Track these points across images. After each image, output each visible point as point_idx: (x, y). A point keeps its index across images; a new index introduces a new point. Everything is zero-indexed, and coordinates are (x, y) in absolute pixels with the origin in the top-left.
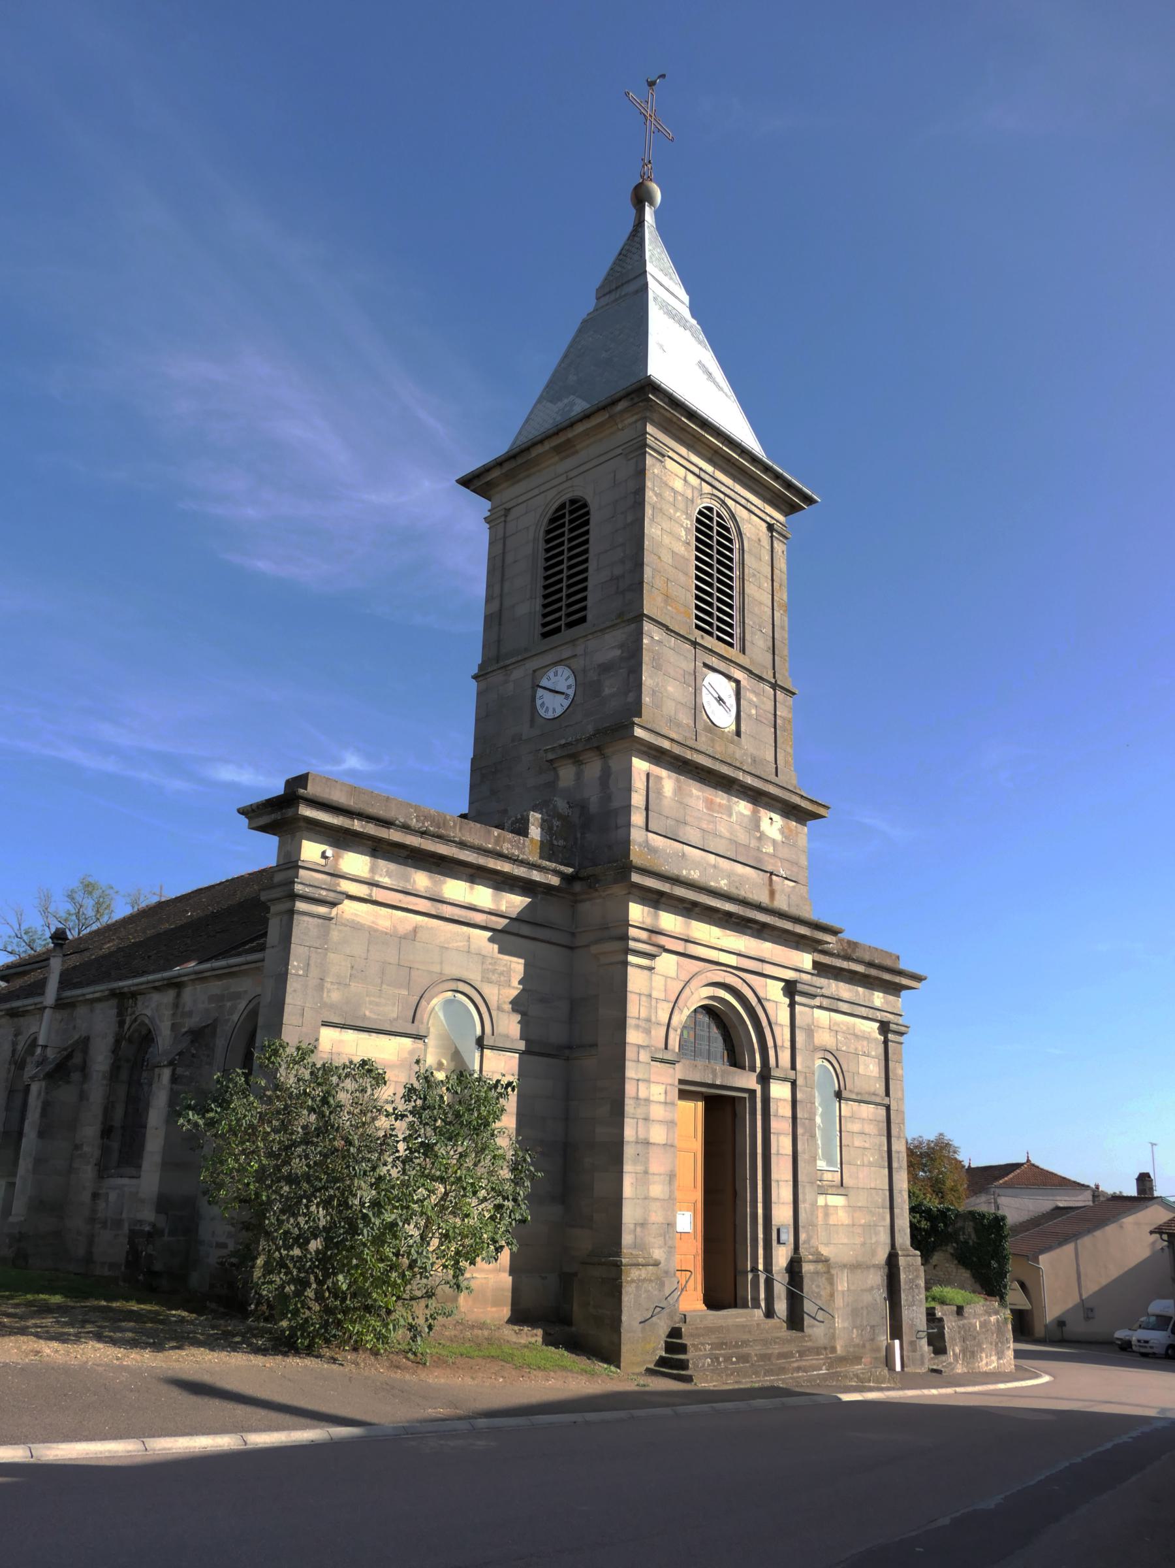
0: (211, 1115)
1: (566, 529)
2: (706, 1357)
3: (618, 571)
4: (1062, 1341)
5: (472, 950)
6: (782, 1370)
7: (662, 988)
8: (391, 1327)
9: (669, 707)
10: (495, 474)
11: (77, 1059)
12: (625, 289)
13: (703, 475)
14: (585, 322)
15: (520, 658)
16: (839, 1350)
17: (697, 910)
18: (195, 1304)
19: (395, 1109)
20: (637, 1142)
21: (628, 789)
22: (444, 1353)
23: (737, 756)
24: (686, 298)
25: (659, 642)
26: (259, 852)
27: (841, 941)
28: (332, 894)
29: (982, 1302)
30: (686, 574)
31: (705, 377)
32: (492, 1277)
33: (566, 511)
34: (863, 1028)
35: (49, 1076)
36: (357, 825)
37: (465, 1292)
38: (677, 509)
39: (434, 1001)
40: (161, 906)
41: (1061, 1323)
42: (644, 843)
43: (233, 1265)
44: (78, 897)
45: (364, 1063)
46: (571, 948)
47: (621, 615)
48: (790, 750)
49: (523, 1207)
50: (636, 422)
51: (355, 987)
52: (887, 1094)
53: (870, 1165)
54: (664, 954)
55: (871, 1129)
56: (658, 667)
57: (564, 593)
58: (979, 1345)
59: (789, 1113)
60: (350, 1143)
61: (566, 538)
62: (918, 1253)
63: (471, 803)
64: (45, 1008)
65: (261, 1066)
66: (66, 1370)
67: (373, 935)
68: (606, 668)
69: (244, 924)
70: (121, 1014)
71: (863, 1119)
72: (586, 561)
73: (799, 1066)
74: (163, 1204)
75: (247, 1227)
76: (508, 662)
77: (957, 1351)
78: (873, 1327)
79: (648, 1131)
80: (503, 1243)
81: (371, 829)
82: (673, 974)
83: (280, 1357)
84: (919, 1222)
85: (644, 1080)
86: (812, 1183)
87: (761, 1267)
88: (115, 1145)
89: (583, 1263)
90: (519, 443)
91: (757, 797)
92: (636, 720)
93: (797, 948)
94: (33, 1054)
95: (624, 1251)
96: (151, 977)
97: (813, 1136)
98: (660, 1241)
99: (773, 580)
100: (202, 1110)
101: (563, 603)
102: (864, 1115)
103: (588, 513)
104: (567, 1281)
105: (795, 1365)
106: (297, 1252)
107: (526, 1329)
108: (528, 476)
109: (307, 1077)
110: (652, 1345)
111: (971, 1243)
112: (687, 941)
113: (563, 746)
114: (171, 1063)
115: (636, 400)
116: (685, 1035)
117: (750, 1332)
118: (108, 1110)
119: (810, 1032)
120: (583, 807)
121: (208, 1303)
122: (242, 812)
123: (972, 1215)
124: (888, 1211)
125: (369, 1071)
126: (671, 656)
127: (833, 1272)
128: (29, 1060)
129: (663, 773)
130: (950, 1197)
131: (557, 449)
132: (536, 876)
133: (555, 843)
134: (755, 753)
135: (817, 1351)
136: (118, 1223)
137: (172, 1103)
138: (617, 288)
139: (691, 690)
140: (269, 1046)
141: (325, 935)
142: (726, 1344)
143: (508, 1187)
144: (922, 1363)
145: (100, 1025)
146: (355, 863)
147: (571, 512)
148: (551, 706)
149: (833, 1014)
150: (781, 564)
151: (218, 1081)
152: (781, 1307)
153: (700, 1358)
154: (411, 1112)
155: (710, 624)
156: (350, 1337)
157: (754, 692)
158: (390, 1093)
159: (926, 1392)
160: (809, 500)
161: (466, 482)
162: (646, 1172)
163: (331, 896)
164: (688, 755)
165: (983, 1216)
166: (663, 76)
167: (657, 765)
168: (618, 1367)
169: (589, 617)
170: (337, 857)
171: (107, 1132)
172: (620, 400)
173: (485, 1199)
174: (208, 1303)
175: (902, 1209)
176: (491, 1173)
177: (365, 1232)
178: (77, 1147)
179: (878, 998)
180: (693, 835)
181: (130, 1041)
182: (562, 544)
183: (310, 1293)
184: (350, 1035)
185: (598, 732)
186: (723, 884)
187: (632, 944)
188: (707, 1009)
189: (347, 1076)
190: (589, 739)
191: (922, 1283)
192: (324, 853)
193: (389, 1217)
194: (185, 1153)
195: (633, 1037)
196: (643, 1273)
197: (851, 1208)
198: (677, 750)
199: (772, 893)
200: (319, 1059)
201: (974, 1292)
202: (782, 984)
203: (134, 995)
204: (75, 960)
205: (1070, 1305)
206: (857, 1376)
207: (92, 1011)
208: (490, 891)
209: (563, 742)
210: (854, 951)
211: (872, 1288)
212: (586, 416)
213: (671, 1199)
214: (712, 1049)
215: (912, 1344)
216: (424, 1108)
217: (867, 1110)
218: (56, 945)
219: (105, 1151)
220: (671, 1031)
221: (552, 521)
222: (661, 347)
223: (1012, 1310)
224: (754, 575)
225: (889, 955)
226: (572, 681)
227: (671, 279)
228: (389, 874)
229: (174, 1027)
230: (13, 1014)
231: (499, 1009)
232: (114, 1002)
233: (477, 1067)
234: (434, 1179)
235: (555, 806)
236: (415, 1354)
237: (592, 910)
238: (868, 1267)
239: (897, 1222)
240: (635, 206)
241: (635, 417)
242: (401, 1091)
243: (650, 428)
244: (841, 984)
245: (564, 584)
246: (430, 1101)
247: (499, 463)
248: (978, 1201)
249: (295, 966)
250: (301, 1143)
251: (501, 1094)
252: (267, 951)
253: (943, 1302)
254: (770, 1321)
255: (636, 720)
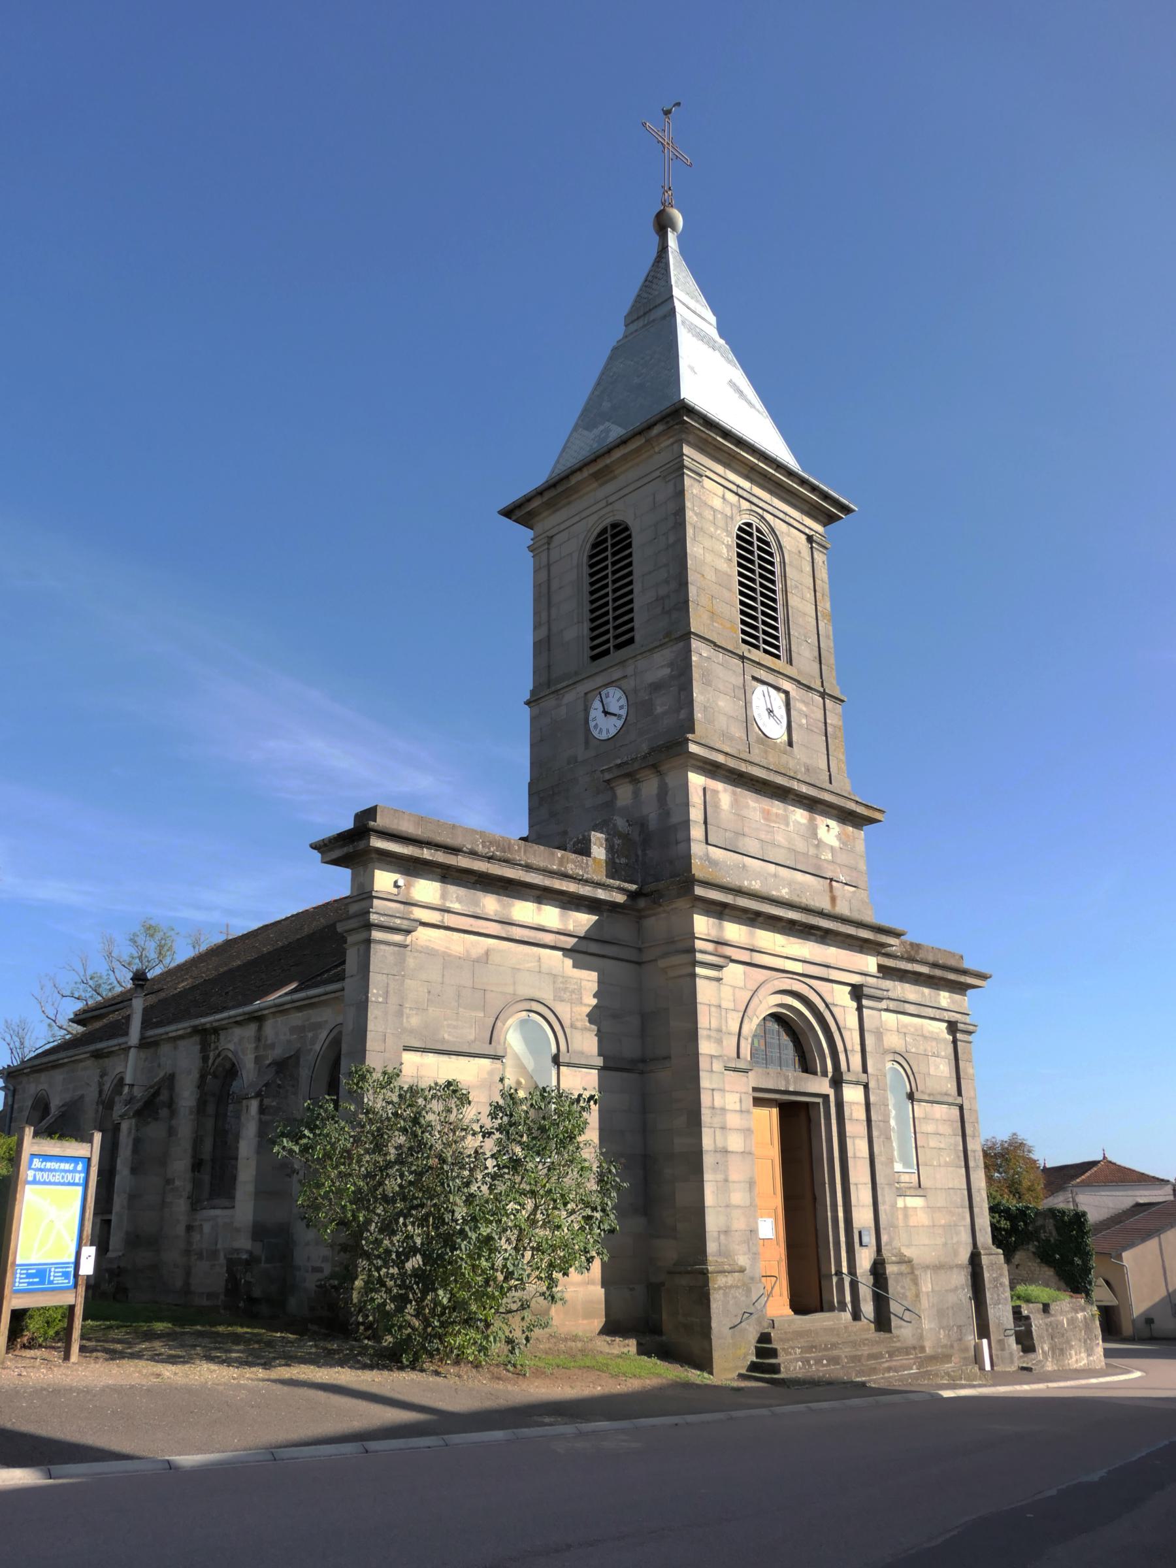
0: (305, 1141)
1: (609, 553)
2: (797, 1360)
3: (663, 591)
4: (1152, 1339)
5: (543, 970)
6: (874, 1370)
7: (731, 998)
8: (491, 1339)
9: (721, 722)
10: (535, 503)
11: (164, 1096)
12: (653, 314)
13: (741, 492)
14: (615, 349)
15: (571, 682)
16: (928, 1345)
17: (761, 919)
18: (300, 1326)
19: (481, 1127)
20: (716, 1151)
21: (686, 805)
22: (541, 1364)
23: (791, 765)
24: (713, 319)
25: (708, 658)
26: (336, 883)
27: (903, 943)
28: (406, 922)
29: (1068, 1299)
30: (730, 590)
31: (737, 395)
32: (584, 1288)
33: (608, 535)
34: (931, 1029)
35: (138, 1114)
36: (427, 854)
37: (560, 1303)
38: (717, 527)
39: (510, 1022)
40: (229, 944)
41: (1149, 1321)
42: (706, 856)
43: (334, 1287)
44: (141, 940)
45: (449, 1084)
46: (639, 963)
47: (668, 634)
48: (843, 757)
49: (612, 1216)
50: (672, 444)
51: (434, 1012)
52: (960, 1093)
53: (947, 1165)
54: (732, 965)
55: (946, 1129)
56: (708, 683)
57: (611, 616)
58: (1068, 1342)
59: (863, 1116)
60: (443, 1161)
61: (609, 562)
62: (1000, 1251)
63: (531, 826)
64: (130, 1048)
65: (350, 1092)
66: (188, 1390)
67: (447, 961)
68: (656, 687)
69: (322, 953)
70: (205, 1048)
71: (937, 1120)
72: (631, 583)
73: (870, 1070)
74: (259, 1232)
75: (344, 1248)
76: (559, 686)
77: (1046, 1348)
78: (959, 1327)
79: (726, 1139)
80: (594, 1254)
81: (440, 857)
82: (741, 984)
83: (386, 1373)
84: (999, 1222)
85: (719, 1090)
86: (890, 1185)
87: (845, 1270)
88: (206, 1178)
89: (669, 1273)
90: (557, 471)
91: (812, 804)
92: (690, 736)
93: (861, 952)
94: (121, 1094)
95: (710, 1258)
96: (232, 1013)
97: (889, 1138)
98: (744, 1248)
99: (815, 591)
100: (296, 1137)
101: (611, 626)
102: (938, 1116)
103: (629, 536)
104: (654, 1291)
105: (886, 1365)
106: (394, 1271)
107: (618, 1339)
108: (569, 503)
109: (395, 1099)
110: (743, 1351)
111: (1052, 1240)
112: (752, 950)
113: (619, 766)
114: (258, 1095)
115: (671, 423)
116: (756, 1044)
117: (838, 1335)
118: (197, 1142)
119: (879, 1035)
120: (642, 824)
121: (309, 1326)
122: (314, 847)
123: (1052, 1213)
124: (967, 1210)
125: (455, 1091)
126: (719, 671)
127: (917, 1272)
128: (117, 1099)
129: (719, 786)
130: (1027, 1196)
131: (596, 476)
132: (601, 894)
133: (617, 861)
134: (808, 762)
135: (907, 1351)
136: (214, 1254)
137: (262, 1133)
138: (645, 314)
139: (742, 703)
140: (356, 1072)
141: (402, 962)
142: (815, 1347)
143: (595, 1199)
144: (1012, 1362)
145: (184, 1062)
146: (426, 890)
147: (613, 536)
148: (604, 727)
149: (900, 1016)
150: (823, 574)
151: (309, 1108)
152: (868, 1308)
153: (791, 1361)
154: (497, 1130)
155: (756, 638)
156: (452, 1352)
157: (803, 702)
158: (477, 1112)
159: (1018, 1387)
160: (847, 510)
161: (508, 513)
162: (726, 1180)
163: (405, 924)
164: (743, 767)
165: (1063, 1213)
166: (678, 104)
167: (713, 778)
168: (711, 1373)
169: (637, 638)
170: (408, 886)
171: (197, 1165)
172: (655, 424)
173: (573, 1212)
174: (309, 1326)
175: (981, 1208)
176: (578, 1185)
177: (463, 1247)
178: (169, 1181)
179: (945, 998)
180: (752, 846)
181: (215, 1076)
182: (606, 567)
183: (410, 1309)
184: (431, 1058)
185: (653, 750)
186: (784, 893)
187: (699, 957)
188: (776, 1017)
189: (433, 1097)
190: (645, 757)
191: (1006, 1281)
192: (396, 882)
193: (485, 1231)
194: (277, 1179)
195: (706, 1047)
196: (729, 1280)
197: (930, 1208)
198: (732, 763)
199: (833, 899)
200: (405, 1081)
201: (1059, 1289)
202: (849, 988)
203: (216, 1031)
204: (152, 999)
205: (1157, 1299)
206: (948, 1374)
207: (175, 1048)
208: (557, 910)
209: (619, 761)
210: (917, 952)
211: (956, 1289)
212: (624, 442)
213: (752, 1205)
214: (783, 1057)
215: (1001, 1342)
216: (511, 1124)
217: (940, 1111)
218: (137, 986)
219: (197, 1184)
220: (742, 1040)
221: (594, 546)
222: (692, 369)
223: (1099, 1307)
224: (797, 587)
225: (953, 955)
226: (623, 701)
227: (697, 301)
228: (459, 900)
229: (258, 1059)
230: (98, 1055)
231: (572, 1026)
232: (197, 1038)
233: (554, 1083)
234: (523, 1193)
235: (615, 825)
236: (514, 1366)
237: (658, 925)
238: (951, 1268)
239: (977, 1221)
240: (657, 233)
241: (671, 440)
242: (486, 1110)
243: (687, 450)
244: (907, 985)
245: (610, 607)
246: (515, 1119)
247: (540, 493)
248: (1056, 1201)
249: (375, 993)
250: (395, 1163)
251: (583, 1108)
252: (347, 980)
253: (1028, 1301)
254: (858, 1323)
255: (690, 736)
